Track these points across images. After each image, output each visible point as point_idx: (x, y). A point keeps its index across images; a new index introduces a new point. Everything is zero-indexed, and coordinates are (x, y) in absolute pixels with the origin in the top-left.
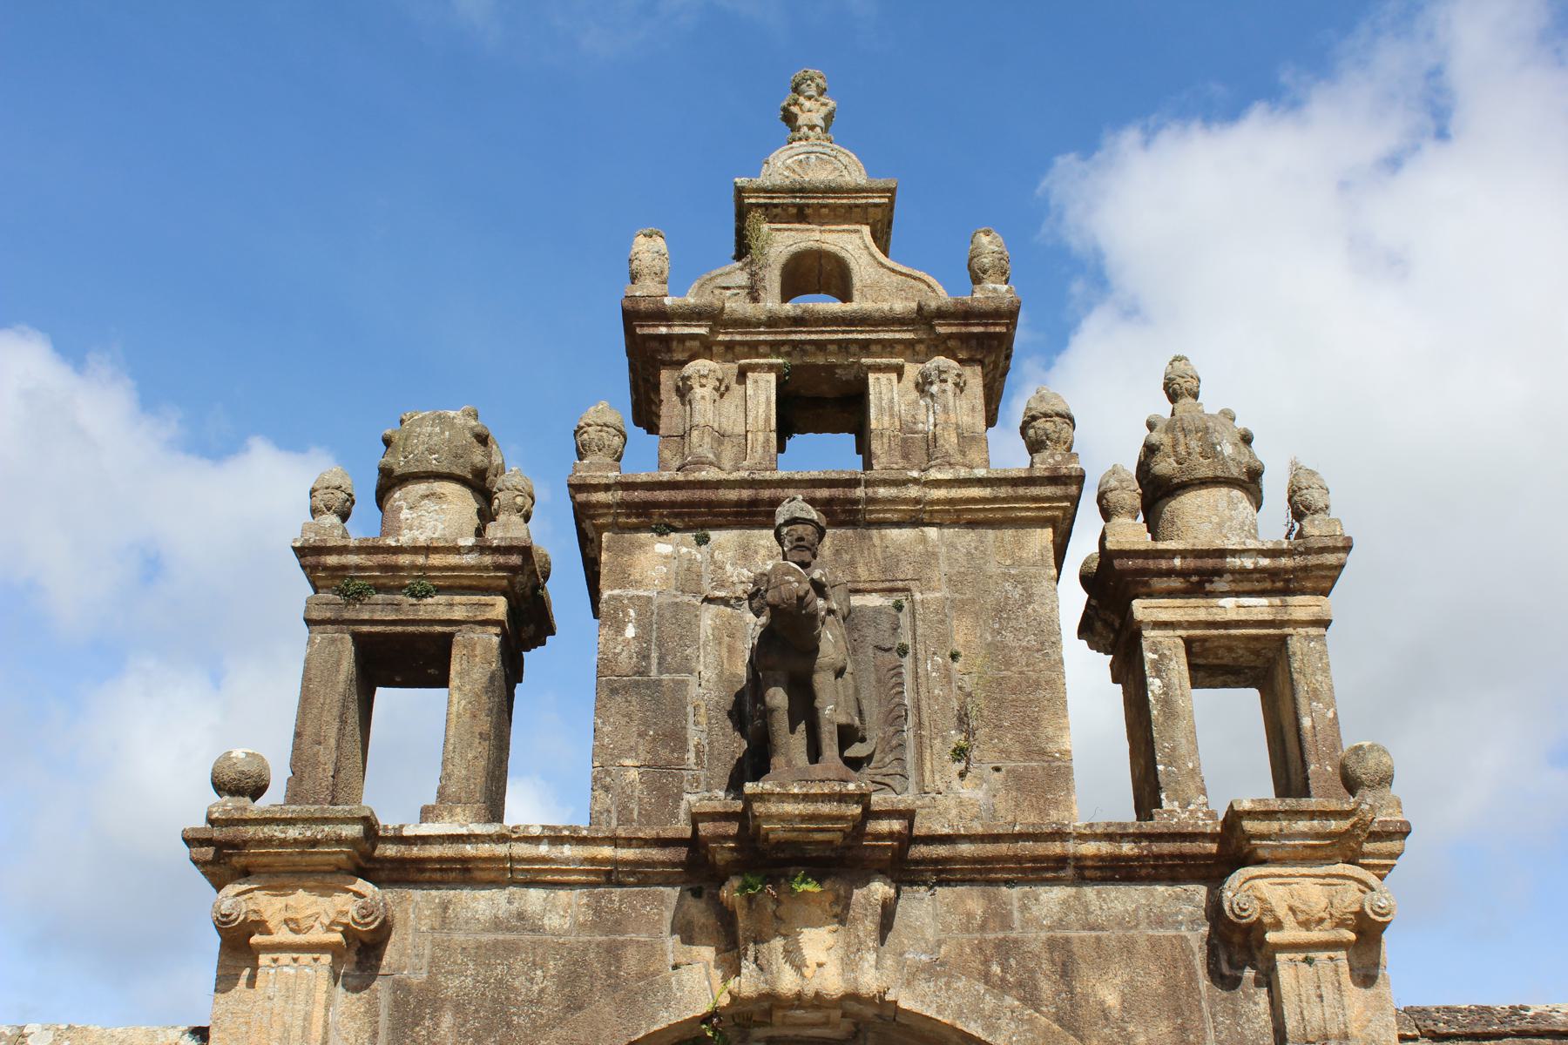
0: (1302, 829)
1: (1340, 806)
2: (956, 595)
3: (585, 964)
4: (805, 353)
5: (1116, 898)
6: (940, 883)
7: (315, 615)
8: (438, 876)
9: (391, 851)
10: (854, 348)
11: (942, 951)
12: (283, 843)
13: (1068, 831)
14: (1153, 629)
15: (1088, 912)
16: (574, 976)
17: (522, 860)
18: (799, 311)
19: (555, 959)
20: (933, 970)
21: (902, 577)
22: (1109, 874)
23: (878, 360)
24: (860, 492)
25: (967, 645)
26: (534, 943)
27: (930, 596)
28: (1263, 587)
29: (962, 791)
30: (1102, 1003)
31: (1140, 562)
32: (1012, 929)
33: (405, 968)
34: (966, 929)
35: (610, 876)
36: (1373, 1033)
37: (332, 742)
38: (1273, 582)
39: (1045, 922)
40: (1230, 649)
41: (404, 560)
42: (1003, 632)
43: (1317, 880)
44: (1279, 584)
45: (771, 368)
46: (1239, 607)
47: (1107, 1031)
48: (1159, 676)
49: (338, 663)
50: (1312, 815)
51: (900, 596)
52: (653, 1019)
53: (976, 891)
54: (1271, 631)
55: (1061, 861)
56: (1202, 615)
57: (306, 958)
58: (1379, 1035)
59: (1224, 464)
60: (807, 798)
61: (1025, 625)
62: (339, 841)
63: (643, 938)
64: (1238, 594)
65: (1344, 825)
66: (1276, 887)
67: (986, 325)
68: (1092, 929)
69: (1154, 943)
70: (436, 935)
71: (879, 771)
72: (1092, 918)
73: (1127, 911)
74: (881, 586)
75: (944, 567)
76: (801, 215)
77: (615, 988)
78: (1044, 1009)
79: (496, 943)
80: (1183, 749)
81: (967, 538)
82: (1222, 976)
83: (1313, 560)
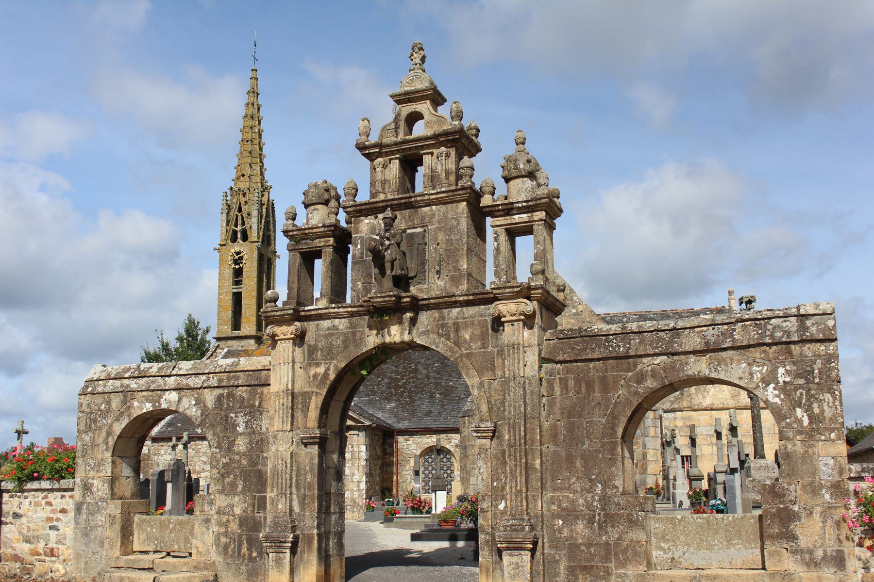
3: (348, 337)
4: (407, 151)
6: (428, 310)
7: (289, 249)
9: (303, 314)
10: (420, 148)
12: (277, 316)
15: (464, 314)
17: (332, 313)
20: (424, 333)
24: (413, 199)
27: (433, 227)
31: (490, 209)
34: (434, 321)
35: (352, 315)
37: (296, 282)
41: (307, 231)
44: (530, 210)
45: (397, 158)
48: (496, 242)
49: (296, 261)
50: (510, 287)
51: (426, 228)
52: (362, 350)
53: (437, 311)
54: (529, 224)
55: (456, 302)
56: (509, 222)
57: (287, 341)
59: (520, 171)
62: (288, 314)
63: (360, 329)
64: (520, 214)
65: (518, 289)
67: (453, 136)
69: (479, 321)
74: (420, 225)
75: (437, 217)
76: (409, 101)
77: (355, 342)
79: (329, 333)
81: (443, 208)
82: (495, 329)
83: (538, 202)
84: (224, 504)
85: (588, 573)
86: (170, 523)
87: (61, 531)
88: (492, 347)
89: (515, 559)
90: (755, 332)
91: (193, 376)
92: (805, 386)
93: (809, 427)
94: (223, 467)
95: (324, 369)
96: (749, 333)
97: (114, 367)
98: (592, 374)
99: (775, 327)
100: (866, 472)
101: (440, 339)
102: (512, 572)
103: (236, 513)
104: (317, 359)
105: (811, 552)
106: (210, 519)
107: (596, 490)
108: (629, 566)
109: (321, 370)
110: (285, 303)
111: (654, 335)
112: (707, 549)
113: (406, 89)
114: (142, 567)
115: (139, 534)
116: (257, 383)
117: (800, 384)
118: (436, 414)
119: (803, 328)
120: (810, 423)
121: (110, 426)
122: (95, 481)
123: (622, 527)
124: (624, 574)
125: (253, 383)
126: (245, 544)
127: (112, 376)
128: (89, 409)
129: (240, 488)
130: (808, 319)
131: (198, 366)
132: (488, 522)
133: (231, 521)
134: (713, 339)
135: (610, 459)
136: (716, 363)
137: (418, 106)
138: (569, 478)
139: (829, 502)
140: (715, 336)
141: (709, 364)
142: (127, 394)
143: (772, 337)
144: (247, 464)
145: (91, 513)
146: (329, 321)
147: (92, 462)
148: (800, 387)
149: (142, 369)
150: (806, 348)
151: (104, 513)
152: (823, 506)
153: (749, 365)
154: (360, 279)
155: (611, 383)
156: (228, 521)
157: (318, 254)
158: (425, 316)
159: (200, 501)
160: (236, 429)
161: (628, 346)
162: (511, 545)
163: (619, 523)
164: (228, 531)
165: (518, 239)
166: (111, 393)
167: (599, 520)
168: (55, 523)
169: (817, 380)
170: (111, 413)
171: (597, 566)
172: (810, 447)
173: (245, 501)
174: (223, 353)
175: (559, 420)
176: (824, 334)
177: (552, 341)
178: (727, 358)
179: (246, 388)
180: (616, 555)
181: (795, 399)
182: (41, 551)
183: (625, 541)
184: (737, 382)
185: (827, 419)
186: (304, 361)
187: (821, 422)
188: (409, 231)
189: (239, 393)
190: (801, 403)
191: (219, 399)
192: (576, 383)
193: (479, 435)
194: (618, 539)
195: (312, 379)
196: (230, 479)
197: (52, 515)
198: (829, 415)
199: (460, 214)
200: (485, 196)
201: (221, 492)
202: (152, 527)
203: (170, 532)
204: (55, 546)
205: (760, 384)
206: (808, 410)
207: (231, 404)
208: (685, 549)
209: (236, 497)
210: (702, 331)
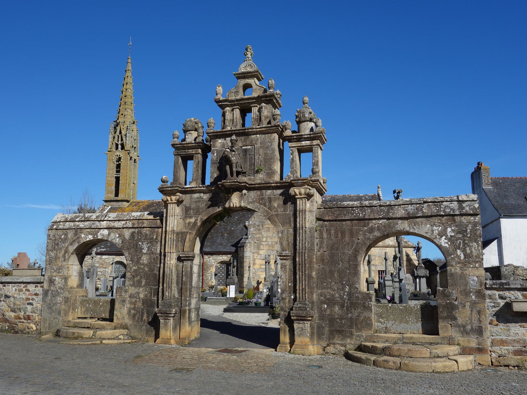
7: (175, 154)
12: (169, 190)
20: (252, 202)
24: (246, 131)
27: (257, 146)
34: (257, 196)
41: (185, 145)
48: (292, 155)
51: (253, 146)
53: (259, 191)
55: (270, 186)
56: (299, 145)
59: (306, 118)
60: (230, 182)
65: (288, 184)
80: (295, 167)
83: (316, 135)
84: (134, 292)
85: (340, 334)
86: (100, 301)
87: (35, 305)
88: (290, 211)
89: (301, 325)
90: (435, 209)
91: (117, 222)
92: (462, 238)
93: (464, 260)
94: (134, 272)
95: (194, 220)
96: (431, 209)
97: (70, 215)
98: (344, 227)
99: (445, 207)
100: (495, 285)
102: (299, 333)
103: (140, 297)
104: (190, 214)
105: (464, 327)
106: (125, 300)
107: (345, 290)
108: (363, 331)
109: (193, 220)
110: (172, 184)
111: (378, 208)
112: (405, 323)
113: (242, 71)
114: (83, 327)
115: (81, 308)
116: (155, 226)
117: (459, 237)
118: (225, 244)
119: (461, 208)
120: (465, 258)
121: (67, 247)
122: (56, 278)
123: (360, 310)
124: (361, 335)
125: (153, 226)
126: (146, 314)
127: (69, 220)
128: (54, 238)
129: (143, 283)
130: (463, 203)
131: (120, 216)
132: (286, 305)
133: (137, 301)
134: (412, 212)
135: (354, 273)
136: (413, 224)
138: (331, 283)
139: (474, 300)
140: (413, 210)
141: (410, 225)
142: (78, 230)
143: (444, 211)
144: (148, 270)
145: (54, 296)
146: (198, 194)
147: (55, 268)
148: (460, 239)
149: (86, 217)
150: (463, 218)
151: (61, 296)
152: (471, 302)
153: (432, 226)
154: (216, 172)
155: (355, 233)
156: (136, 301)
157: (191, 157)
158: (252, 193)
159: (120, 290)
160: (142, 251)
161: (364, 213)
162: (299, 318)
163: (358, 307)
164: (136, 307)
165: (302, 154)
166: (68, 229)
167: (347, 306)
168: (31, 301)
169: (469, 235)
170: (68, 240)
171: (346, 330)
172: (464, 271)
173: (146, 291)
174: (108, 209)
175: (325, 252)
176: (473, 211)
177: (321, 210)
178: (419, 222)
180: (356, 325)
181: (456, 245)
182: (22, 317)
183: (361, 317)
184: (425, 235)
185: (474, 256)
186: (183, 215)
187: (470, 258)
188: (244, 148)
189: (144, 231)
190: (460, 247)
191: (132, 234)
192: (335, 232)
193: (282, 258)
194: (357, 316)
195: (187, 225)
196: (138, 278)
197: (29, 297)
198: (475, 254)
200: (288, 130)
201: (132, 286)
202: (89, 304)
203: (100, 307)
204: (30, 314)
205: (437, 236)
206: (464, 251)
207: (140, 237)
208: (393, 322)
209: (141, 288)
210: (405, 207)
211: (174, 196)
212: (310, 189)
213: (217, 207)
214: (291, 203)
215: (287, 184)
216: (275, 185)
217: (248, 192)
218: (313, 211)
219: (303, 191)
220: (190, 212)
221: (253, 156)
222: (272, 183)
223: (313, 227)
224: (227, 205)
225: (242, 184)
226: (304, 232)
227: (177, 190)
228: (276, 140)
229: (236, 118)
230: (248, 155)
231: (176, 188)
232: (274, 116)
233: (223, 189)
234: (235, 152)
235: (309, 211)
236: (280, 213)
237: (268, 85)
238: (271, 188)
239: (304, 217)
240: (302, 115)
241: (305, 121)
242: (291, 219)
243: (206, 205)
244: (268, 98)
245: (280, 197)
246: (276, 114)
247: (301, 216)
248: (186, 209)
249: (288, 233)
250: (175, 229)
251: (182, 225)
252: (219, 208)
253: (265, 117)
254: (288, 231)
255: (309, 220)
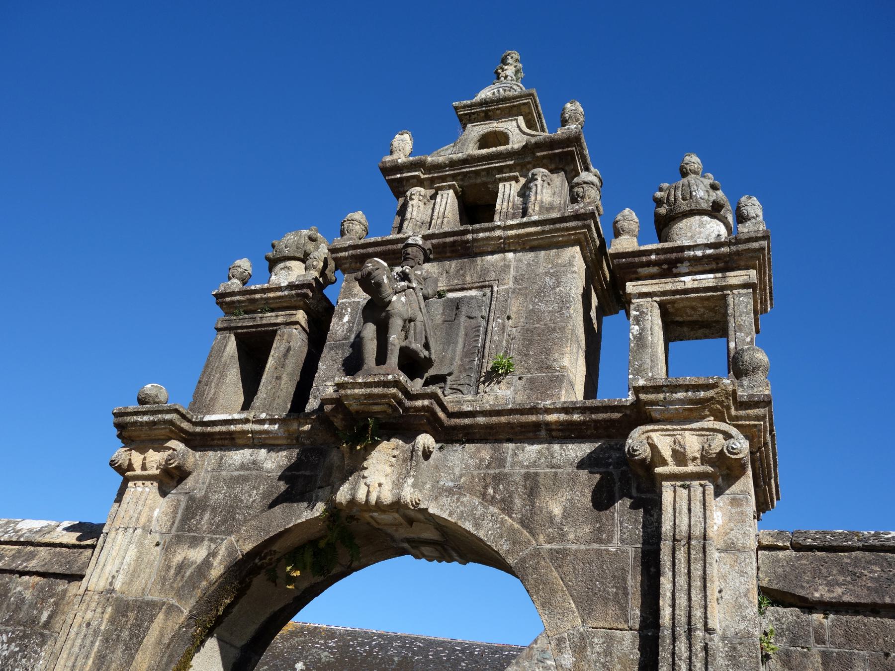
0: (679, 397)
1: (706, 381)
2: (517, 286)
5: (572, 449)
8: (220, 442)
11: (462, 480)
13: (540, 407)
14: (638, 298)
16: (270, 493)
18: (465, 156)
19: (264, 484)
20: (450, 491)
21: (489, 279)
22: (567, 434)
23: (504, 175)
24: (469, 237)
25: (517, 313)
26: (257, 476)
27: (502, 288)
28: (710, 267)
29: (499, 391)
30: (550, 513)
32: (505, 467)
33: (196, 489)
34: (478, 467)
36: (734, 538)
38: (717, 264)
39: (525, 464)
40: (694, 308)
41: (258, 296)
42: (540, 304)
43: (693, 433)
44: (721, 265)
46: (693, 280)
47: (550, 530)
48: (638, 324)
51: (488, 291)
53: (488, 446)
55: (537, 426)
56: (669, 287)
57: (148, 483)
58: (738, 539)
59: (697, 202)
61: (553, 299)
63: (308, 473)
66: (665, 437)
68: (553, 467)
70: (214, 473)
71: (456, 382)
72: (554, 461)
73: (577, 457)
74: (477, 285)
75: (512, 271)
78: (514, 516)
83: (741, 247)
88: (623, 541)
95: (206, 554)
101: (486, 508)
104: (197, 530)
109: (198, 555)
137: (501, 125)
146: (247, 452)
177: (781, 554)
179: (36, 579)
186: (170, 530)
188: (451, 295)
189: (19, 589)
195: (172, 572)
199: (565, 266)
211: (157, 450)
212: (728, 436)
213: (306, 504)
214: (628, 502)
215: (616, 415)
216: (563, 417)
217: (441, 448)
218: (742, 550)
219: (692, 443)
220: (199, 522)
221: (483, 323)
222: (548, 411)
223: (750, 636)
224: (343, 495)
225: (419, 403)
226: (702, 655)
227: (171, 422)
228: (575, 269)
229: (441, 214)
230: (463, 319)
231: (168, 417)
232: (576, 190)
233: (338, 422)
234: (410, 281)
235: (720, 544)
236: (574, 547)
237: (563, 114)
238: (543, 433)
239: (697, 573)
240: (679, 194)
241: (691, 213)
242: (630, 582)
243: (264, 497)
244: (557, 151)
245: (577, 475)
246: (586, 180)
247: (682, 568)
248: (187, 508)
249: (608, 653)
250: (118, 586)
251: (155, 571)
252: (312, 506)
253: (541, 207)
254: (609, 641)
255: (726, 595)
